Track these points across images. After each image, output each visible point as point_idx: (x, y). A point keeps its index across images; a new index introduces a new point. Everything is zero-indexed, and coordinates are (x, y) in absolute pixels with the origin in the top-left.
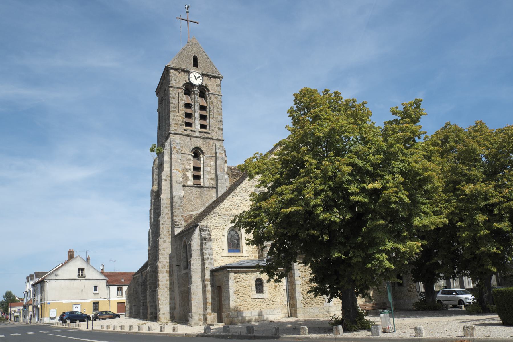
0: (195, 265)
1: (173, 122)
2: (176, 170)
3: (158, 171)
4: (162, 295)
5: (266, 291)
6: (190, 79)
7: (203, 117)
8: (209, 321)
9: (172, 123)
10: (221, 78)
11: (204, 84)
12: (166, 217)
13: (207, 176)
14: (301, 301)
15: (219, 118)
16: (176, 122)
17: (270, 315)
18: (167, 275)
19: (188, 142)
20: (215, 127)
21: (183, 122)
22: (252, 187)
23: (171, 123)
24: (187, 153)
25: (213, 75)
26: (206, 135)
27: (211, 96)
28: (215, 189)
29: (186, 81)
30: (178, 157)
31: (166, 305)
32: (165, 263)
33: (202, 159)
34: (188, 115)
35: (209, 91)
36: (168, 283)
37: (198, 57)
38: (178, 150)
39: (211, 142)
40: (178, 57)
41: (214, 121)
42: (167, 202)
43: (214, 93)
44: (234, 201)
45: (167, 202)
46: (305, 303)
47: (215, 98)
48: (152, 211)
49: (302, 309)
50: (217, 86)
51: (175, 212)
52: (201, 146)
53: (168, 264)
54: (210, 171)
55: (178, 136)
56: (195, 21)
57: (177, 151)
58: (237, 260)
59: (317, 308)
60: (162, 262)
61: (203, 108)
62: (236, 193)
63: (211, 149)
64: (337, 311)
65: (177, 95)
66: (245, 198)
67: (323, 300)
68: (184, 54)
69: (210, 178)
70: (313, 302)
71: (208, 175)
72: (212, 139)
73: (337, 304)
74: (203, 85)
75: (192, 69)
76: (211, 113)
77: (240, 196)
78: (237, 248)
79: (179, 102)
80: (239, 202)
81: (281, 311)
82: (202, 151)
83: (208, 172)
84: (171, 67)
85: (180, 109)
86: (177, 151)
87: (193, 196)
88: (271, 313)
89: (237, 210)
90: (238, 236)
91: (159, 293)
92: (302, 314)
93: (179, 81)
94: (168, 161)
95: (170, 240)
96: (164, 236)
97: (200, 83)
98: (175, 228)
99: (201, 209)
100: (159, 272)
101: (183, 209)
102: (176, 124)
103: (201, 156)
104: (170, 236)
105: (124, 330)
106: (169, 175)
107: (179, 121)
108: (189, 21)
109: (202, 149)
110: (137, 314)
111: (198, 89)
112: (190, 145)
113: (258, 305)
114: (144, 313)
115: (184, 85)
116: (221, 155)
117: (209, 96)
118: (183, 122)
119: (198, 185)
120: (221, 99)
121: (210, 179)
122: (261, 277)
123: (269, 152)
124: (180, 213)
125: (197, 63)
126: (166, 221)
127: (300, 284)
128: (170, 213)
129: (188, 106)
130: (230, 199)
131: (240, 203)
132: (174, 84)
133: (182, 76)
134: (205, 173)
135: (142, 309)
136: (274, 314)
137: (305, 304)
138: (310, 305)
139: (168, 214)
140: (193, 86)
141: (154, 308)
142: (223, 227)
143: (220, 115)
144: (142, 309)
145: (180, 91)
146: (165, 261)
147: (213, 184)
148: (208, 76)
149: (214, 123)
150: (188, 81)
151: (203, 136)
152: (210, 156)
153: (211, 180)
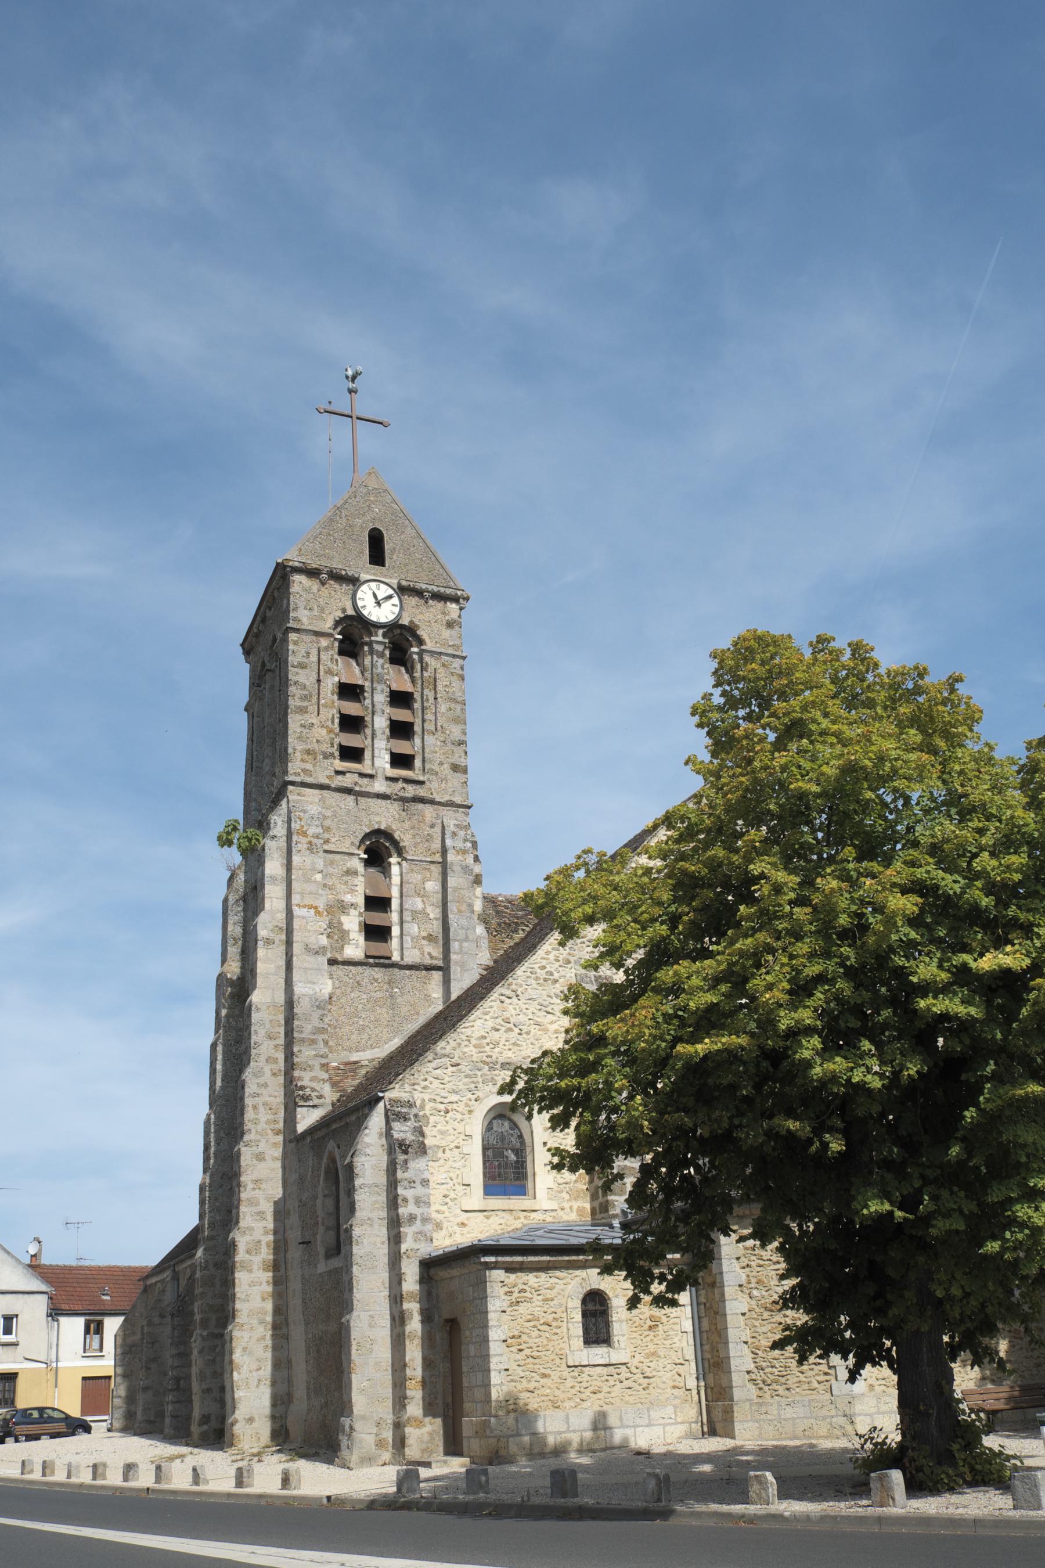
1: (300, 747)
2: (305, 906)
4: (245, 1349)
5: (621, 1338)
6: (360, 604)
7: (400, 730)
9: (295, 749)
10: (461, 601)
11: (405, 621)
12: (267, 1070)
13: (413, 929)
14: (747, 1377)
15: (455, 732)
16: (308, 747)
17: (635, 1427)
19: (349, 811)
20: (441, 764)
21: (332, 745)
22: (569, 966)
23: (290, 750)
24: (347, 851)
25: (436, 589)
26: (411, 791)
28: (441, 973)
29: (344, 610)
30: (313, 864)
31: (257, 1386)
33: (395, 870)
34: (351, 724)
35: (420, 642)
39: (428, 811)
40: (321, 533)
41: (439, 743)
43: (439, 650)
44: (506, 1014)
45: (271, 1017)
46: (762, 1385)
47: (444, 665)
49: (751, 1405)
50: (450, 625)
51: (300, 1051)
52: (394, 827)
53: (271, 1238)
54: (423, 912)
55: (316, 791)
57: (310, 843)
58: (518, 1224)
59: (806, 1403)
60: (251, 1229)
61: (400, 699)
62: (514, 987)
63: (428, 835)
64: (878, 1413)
65: (314, 658)
66: (545, 1003)
67: (826, 1374)
69: (424, 934)
70: (792, 1381)
71: (416, 926)
72: (432, 802)
73: (878, 1389)
74: (400, 622)
75: (366, 571)
77: (527, 996)
78: (517, 1179)
79: (319, 681)
80: (522, 1018)
81: (675, 1412)
82: (395, 843)
83: (415, 913)
84: (297, 564)
85: (322, 702)
87: (364, 996)
88: (638, 1421)
89: (518, 1045)
91: (234, 1344)
92: (750, 1424)
93: (322, 610)
96: (259, 1137)
97: (391, 617)
98: (299, 1109)
99: (391, 1043)
100: (238, 1265)
101: (326, 1043)
102: (308, 752)
103: (393, 860)
106: (280, 925)
107: (318, 741)
109: (396, 836)
110: (152, 1419)
111: (384, 635)
112: (356, 821)
113: (590, 1389)
114: (177, 1417)
115: (337, 623)
116: (460, 857)
117: (421, 660)
118: (332, 745)
119: (382, 961)
120: (462, 668)
121: (424, 938)
122: (602, 1288)
123: (625, 846)
124: (316, 1056)
126: (265, 1085)
127: (743, 1314)
129: (349, 691)
130: (491, 1007)
131: (528, 1022)
132: (305, 620)
133: (333, 593)
134: (407, 916)
135: (173, 1402)
136: (649, 1425)
137: (760, 1389)
138: (781, 1390)
139: (276, 1061)
140: (367, 625)
141: (216, 1400)
142: (467, 1105)
143: (461, 720)
144: (173, 1402)
145: (324, 642)
147: (435, 954)
148: (419, 593)
149: (437, 749)
150: (351, 612)
151: (401, 794)
152: (423, 859)
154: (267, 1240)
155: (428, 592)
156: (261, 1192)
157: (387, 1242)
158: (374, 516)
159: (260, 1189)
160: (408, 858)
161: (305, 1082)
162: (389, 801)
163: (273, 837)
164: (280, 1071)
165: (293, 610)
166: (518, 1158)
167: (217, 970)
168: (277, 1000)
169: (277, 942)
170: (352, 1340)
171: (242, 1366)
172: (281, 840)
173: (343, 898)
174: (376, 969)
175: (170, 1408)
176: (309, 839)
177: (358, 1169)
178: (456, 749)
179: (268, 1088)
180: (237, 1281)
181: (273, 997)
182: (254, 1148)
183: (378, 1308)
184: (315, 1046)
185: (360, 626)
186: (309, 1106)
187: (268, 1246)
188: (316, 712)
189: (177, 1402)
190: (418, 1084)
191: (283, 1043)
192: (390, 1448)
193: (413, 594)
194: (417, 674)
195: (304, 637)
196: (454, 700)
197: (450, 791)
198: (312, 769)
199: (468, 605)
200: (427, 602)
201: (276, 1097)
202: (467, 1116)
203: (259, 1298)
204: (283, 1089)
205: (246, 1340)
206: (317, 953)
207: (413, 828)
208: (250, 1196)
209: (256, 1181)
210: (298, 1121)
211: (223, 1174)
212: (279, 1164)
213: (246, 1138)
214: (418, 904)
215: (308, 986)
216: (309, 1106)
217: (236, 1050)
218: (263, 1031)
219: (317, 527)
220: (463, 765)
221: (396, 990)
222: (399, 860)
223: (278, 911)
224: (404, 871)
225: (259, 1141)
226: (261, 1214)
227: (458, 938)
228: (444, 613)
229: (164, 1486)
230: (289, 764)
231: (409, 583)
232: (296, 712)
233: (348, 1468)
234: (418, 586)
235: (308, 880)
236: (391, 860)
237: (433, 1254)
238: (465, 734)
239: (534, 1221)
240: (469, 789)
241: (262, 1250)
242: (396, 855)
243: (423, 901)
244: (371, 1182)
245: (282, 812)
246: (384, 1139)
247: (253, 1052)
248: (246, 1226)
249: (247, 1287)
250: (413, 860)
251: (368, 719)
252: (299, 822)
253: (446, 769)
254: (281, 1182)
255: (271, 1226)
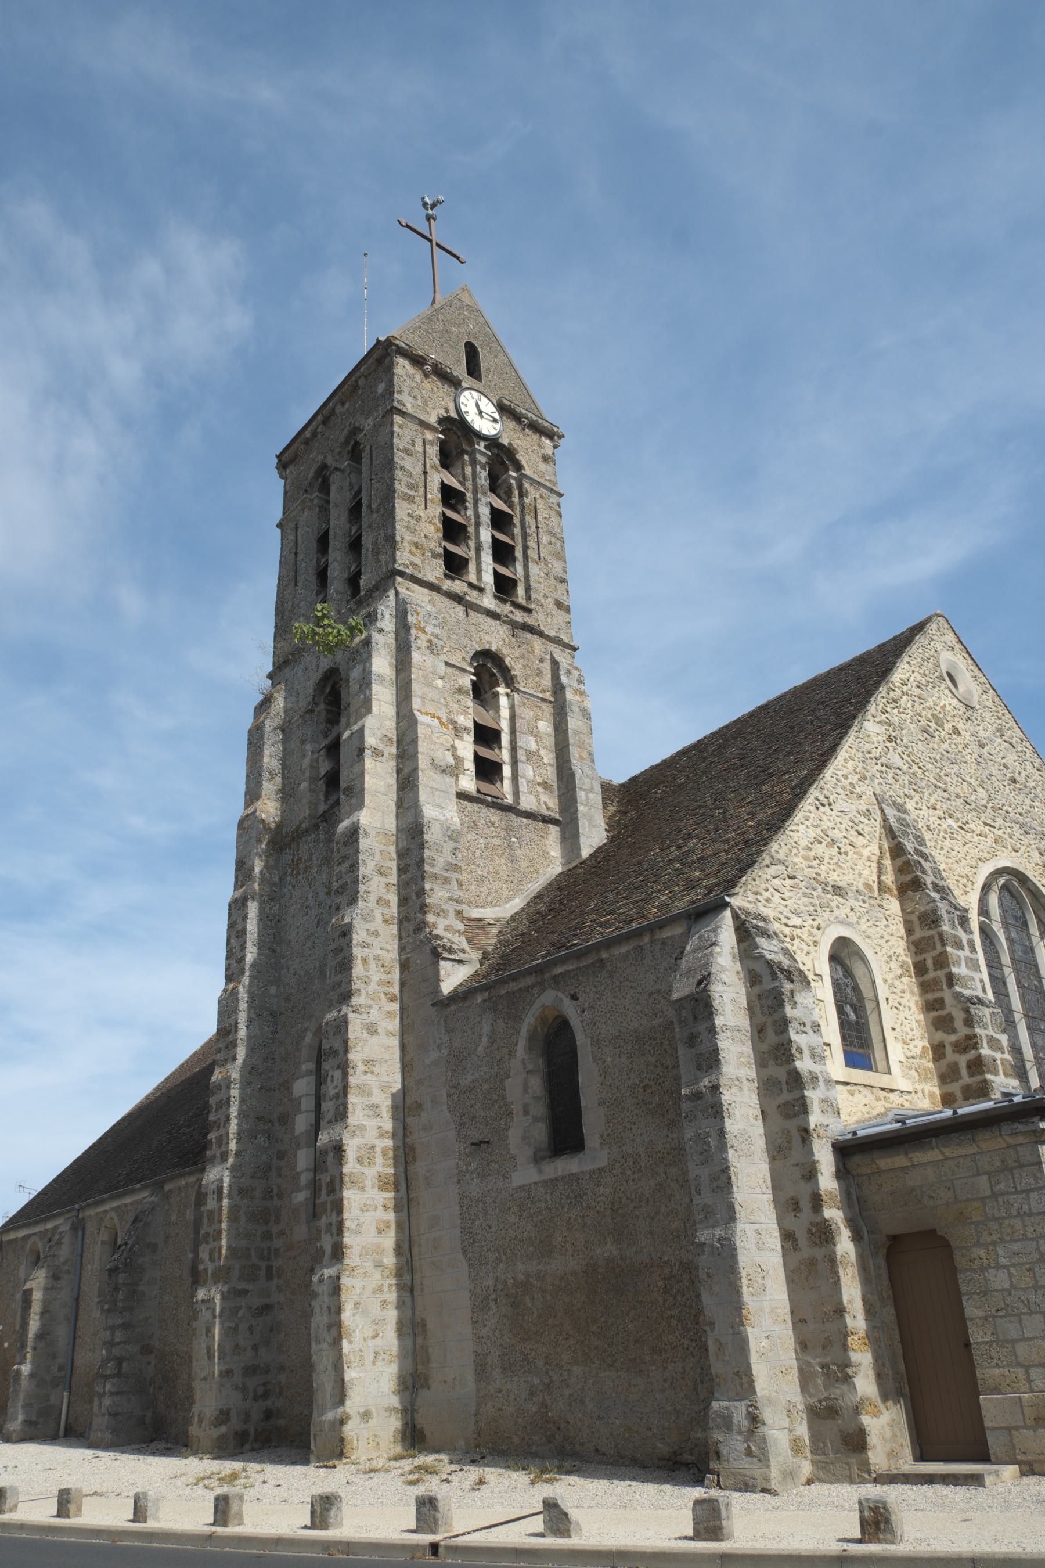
0: (737, 1112)
1: (408, 537)
2: (427, 714)
3: (284, 742)
4: (357, 1305)
6: (463, 409)
7: (502, 553)
8: (879, 1449)
9: (403, 539)
10: (556, 438)
12: (378, 914)
13: (527, 770)
15: (557, 567)
16: (416, 540)
18: (381, 1202)
19: (459, 622)
20: (545, 596)
23: (398, 538)
25: (535, 418)
27: (527, 485)
28: (558, 828)
29: (447, 411)
31: (374, 1363)
32: (371, 1137)
33: (503, 701)
34: (453, 531)
35: (519, 467)
36: (389, 1241)
37: (479, 349)
38: (435, 641)
40: (420, 327)
41: (542, 574)
42: (382, 847)
45: (382, 847)
48: (253, 909)
50: (546, 459)
51: (432, 890)
52: (504, 651)
53: (389, 1143)
56: (454, 252)
57: (430, 641)
58: (879, 1108)
60: (362, 1128)
65: (419, 448)
66: (857, 821)
68: (439, 326)
69: (539, 780)
72: (541, 634)
75: (467, 381)
76: (532, 544)
82: (505, 671)
83: (529, 754)
85: (429, 496)
86: (430, 641)
87: (482, 841)
90: (856, 989)
91: (343, 1298)
93: (426, 403)
94: (388, 679)
95: (395, 1025)
96: (370, 1002)
97: (493, 432)
98: (442, 963)
99: (513, 903)
100: (346, 1179)
101: (460, 884)
102: (416, 545)
103: (502, 690)
104: (396, 1006)
105: (241, 1523)
106: (390, 735)
107: (426, 537)
108: (438, 245)
110: (34, 1419)
111: (486, 447)
114: (116, 1415)
116: (577, 698)
117: (520, 487)
120: (559, 505)
121: (539, 784)
124: (450, 899)
125: (478, 365)
126: (376, 934)
128: (396, 899)
129: (450, 497)
132: (409, 406)
133: (435, 388)
134: (521, 755)
135: (111, 1394)
139: (387, 903)
141: (236, 1388)
142: (811, 934)
143: (561, 557)
144: (111, 1394)
145: (429, 436)
146: (372, 1124)
147: (551, 805)
149: (542, 580)
152: (536, 694)
153: (540, 789)
154: (383, 1145)
155: (527, 418)
156: (374, 1078)
157: (760, 1117)
158: (468, 331)
159: (372, 1073)
160: (522, 689)
161: (439, 931)
162: (498, 622)
163: (381, 630)
164: (392, 917)
165: (398, 392)
166: (857, 1018)
167: (237, 809)
168: (387, 826)
169: (386, 755)
170: (741, 1270)
171: (354, 1331)
172: (389, 636)
173: (456, 719)
174: (493, 810)
175: (107, 1401)
176: (429, 637)
177: (717, 1002)
178: (559, 585)
179: (379, 938)
180: (345, 1202)
181: (383, 822)
182: (365, 1016)
183: (763, 1220)
184: (448, 886)
185: (459, 434)
186: (454, 960)
187: (384, 1154)
188: (423, 506)
189: (117, 1393)
190: (761, 894)
191: (395, 882)
192: (809, 1454)
193: (511, 417)
194: (516, 499)
195: (409, 424)
196: (554, 535)
197: (556, 627)
198: (421, 565)
199: (562, 442)
200: (524, 430)
201: (388, 951)
202: (812, 948)
203: (373, 1230)
204: (396, 941)
205: (358, 1291)
206: (444, 771)
207: (523, 657)
208: (360, 1082)
209: (368, 1062)
210: (442, 978)
211: (253, 1068)
212: (395, 1042)
213: (354, 1001)
214: (532, 744)
215: (437, 809)
216: (454, 960)
217: (271, 909)
218: (373, 863)
219: (417, 320)
220: (566, 603)
221: (514, 839)
222: (509, 691)
223: (388, 719)
224: (516, 703)
225: (370, 1007)
226: (374, 1107)
227: (584, 787)
228: (539, 446)
229: (232, 1530)
230: (397, 552)
231: (509, 403)
232: (403, 499)
233: (764, 1490)
234: (518, 409)
235: (429, 685)
236: (499, 689)
237: (861, 1133)
238: (566, 573)
239: (894, 1106)
240: (573, 630)
241: (377, 1160)
242: (503, 685)
243: (536, 741)
244: (733, 1024)
245: (389, 603)
246: (738, 963)
247: (362, 888)
248: (356, 1123)
249: (358, 1212)
250: (525, 693)
251: (471, 530)
252: (415, 616)
253: (550, 604)
254: (398, 1065)
255: (388, 1126)
